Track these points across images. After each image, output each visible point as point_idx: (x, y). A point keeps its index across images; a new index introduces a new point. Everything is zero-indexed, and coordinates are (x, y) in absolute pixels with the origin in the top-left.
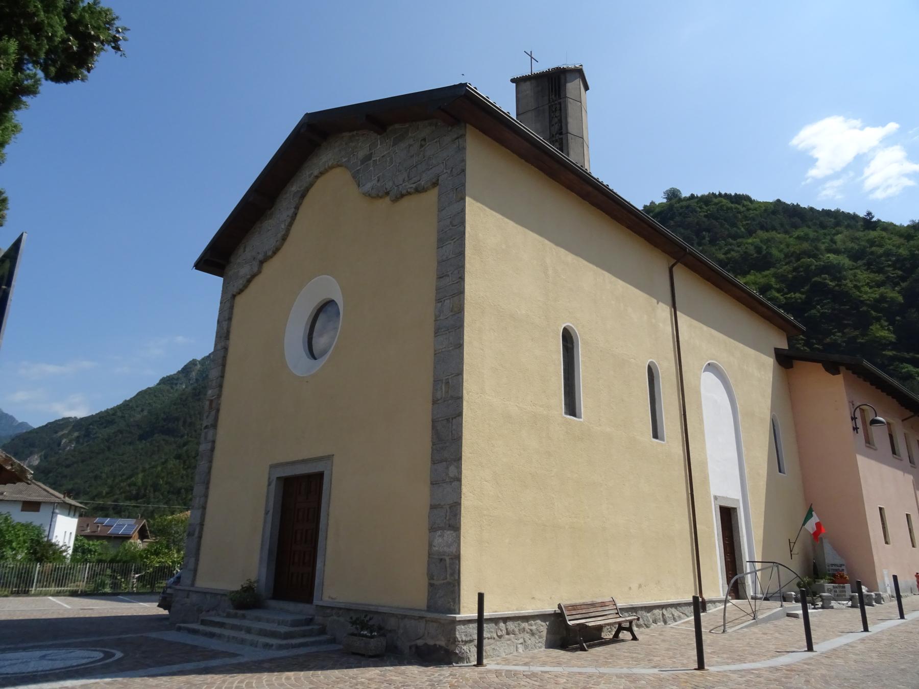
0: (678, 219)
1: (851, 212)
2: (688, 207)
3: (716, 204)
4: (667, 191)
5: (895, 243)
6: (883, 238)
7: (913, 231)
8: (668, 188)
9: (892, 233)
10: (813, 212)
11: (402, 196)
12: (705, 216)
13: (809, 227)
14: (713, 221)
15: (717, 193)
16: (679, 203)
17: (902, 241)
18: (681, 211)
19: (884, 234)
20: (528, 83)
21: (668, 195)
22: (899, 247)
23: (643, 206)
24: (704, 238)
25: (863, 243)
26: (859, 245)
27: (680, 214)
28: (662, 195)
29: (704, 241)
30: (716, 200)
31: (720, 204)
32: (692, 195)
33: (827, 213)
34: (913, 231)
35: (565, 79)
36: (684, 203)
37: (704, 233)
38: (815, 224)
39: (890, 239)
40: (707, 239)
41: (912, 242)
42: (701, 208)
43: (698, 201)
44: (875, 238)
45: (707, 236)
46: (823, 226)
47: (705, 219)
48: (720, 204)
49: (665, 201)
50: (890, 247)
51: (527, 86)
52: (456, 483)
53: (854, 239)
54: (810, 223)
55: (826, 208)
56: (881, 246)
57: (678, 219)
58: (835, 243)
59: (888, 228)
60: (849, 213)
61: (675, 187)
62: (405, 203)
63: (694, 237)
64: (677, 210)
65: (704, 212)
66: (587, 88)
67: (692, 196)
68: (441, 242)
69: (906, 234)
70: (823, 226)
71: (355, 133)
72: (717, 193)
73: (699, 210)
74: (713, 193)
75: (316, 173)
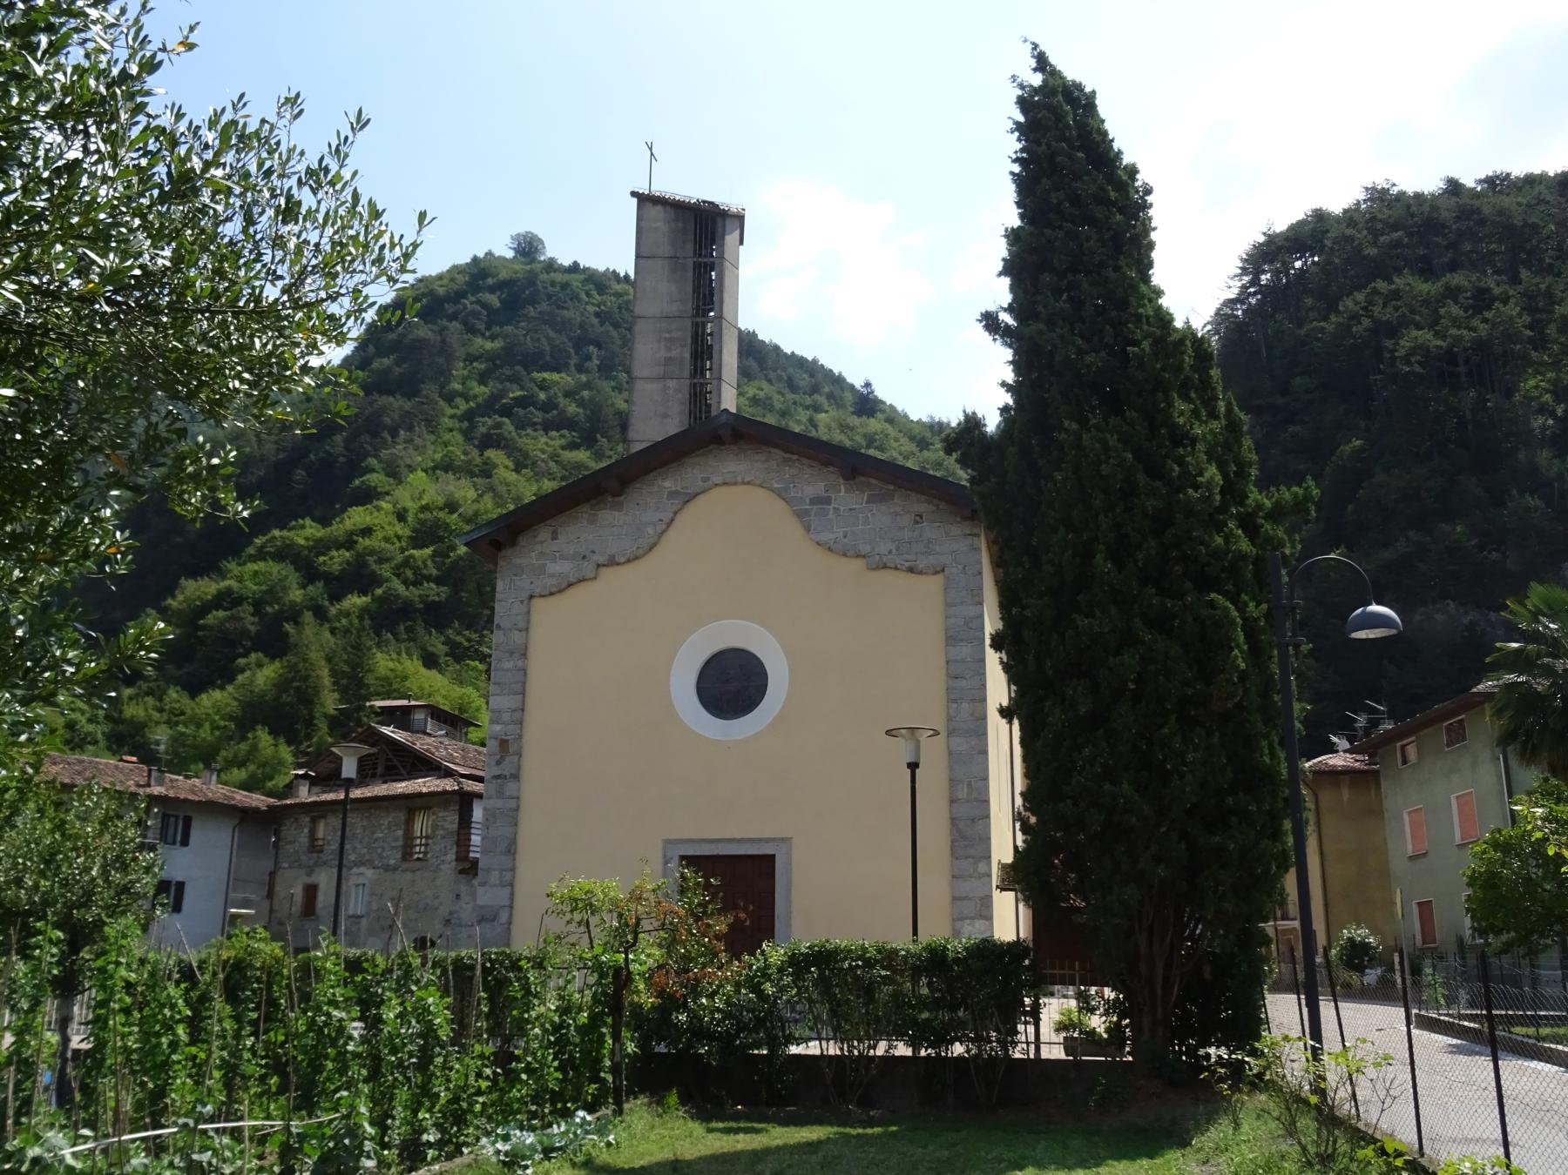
0: (544, 306)
1: (836, 371)
2: (565, 286)
3: (618, 295)
4: (518, 235)
5: (903, 449)
6: (887, 436)
7: (929, 435)
8: (522, 230)
9: (900, 431)
10: (778, 355)
11: (885, 567)
12: (597, 315)
13: (770, 381)
14: (611, 328)
15: (622, 274)
16: (548, 273)
17: (912, 447)
18: (550, 289)
19: (890, 430)
20: (659, 208)
21: (519, 244)
22: (907, 458)
23: (471, 256)
24: (588, 358)
25: (858, 438)
26: (851, 440)
27: (549, 297)
28: (508, 241)
29: (588, 364)
30: (618, 287)
31: (626, 298)
32: (576, 264)
33: (799, 362)
34: (929, 435)
35: (724, 226)
36: (558, 277)
37: (591, 348)
38: (780, 379)
39: (897, 440)
40: (596, 362)
41: (926, 453)
42: (588, 295)
43: (586, 280)
44: (876, 434)
45: (594, 356)
46: (792, 386)
47: (595, 321)
48: (626, 298)
49: (510, 254)
50: (895, 454)
51: (656, 212)
52: (986, 879)
53: (844, 428)
54: (772, 375)
55: (799, 352)
56: (881, 449)
57: (544, 306)
58: (816, 427)
59: (894, 417)
60: (831, 371)
61: (535, 232)
62: (888, 576)
63: (572, 351)
64: (545, 288)
65: (593, 304)
66: (741, 242)
67: (575, 268)
68: (951, 639)
69: (919, 437)
70: (792, 386)
71: (795, 457)
72: (622, 274)
73: (583, 296)
74: (614, 271)
75: (718, 480)
